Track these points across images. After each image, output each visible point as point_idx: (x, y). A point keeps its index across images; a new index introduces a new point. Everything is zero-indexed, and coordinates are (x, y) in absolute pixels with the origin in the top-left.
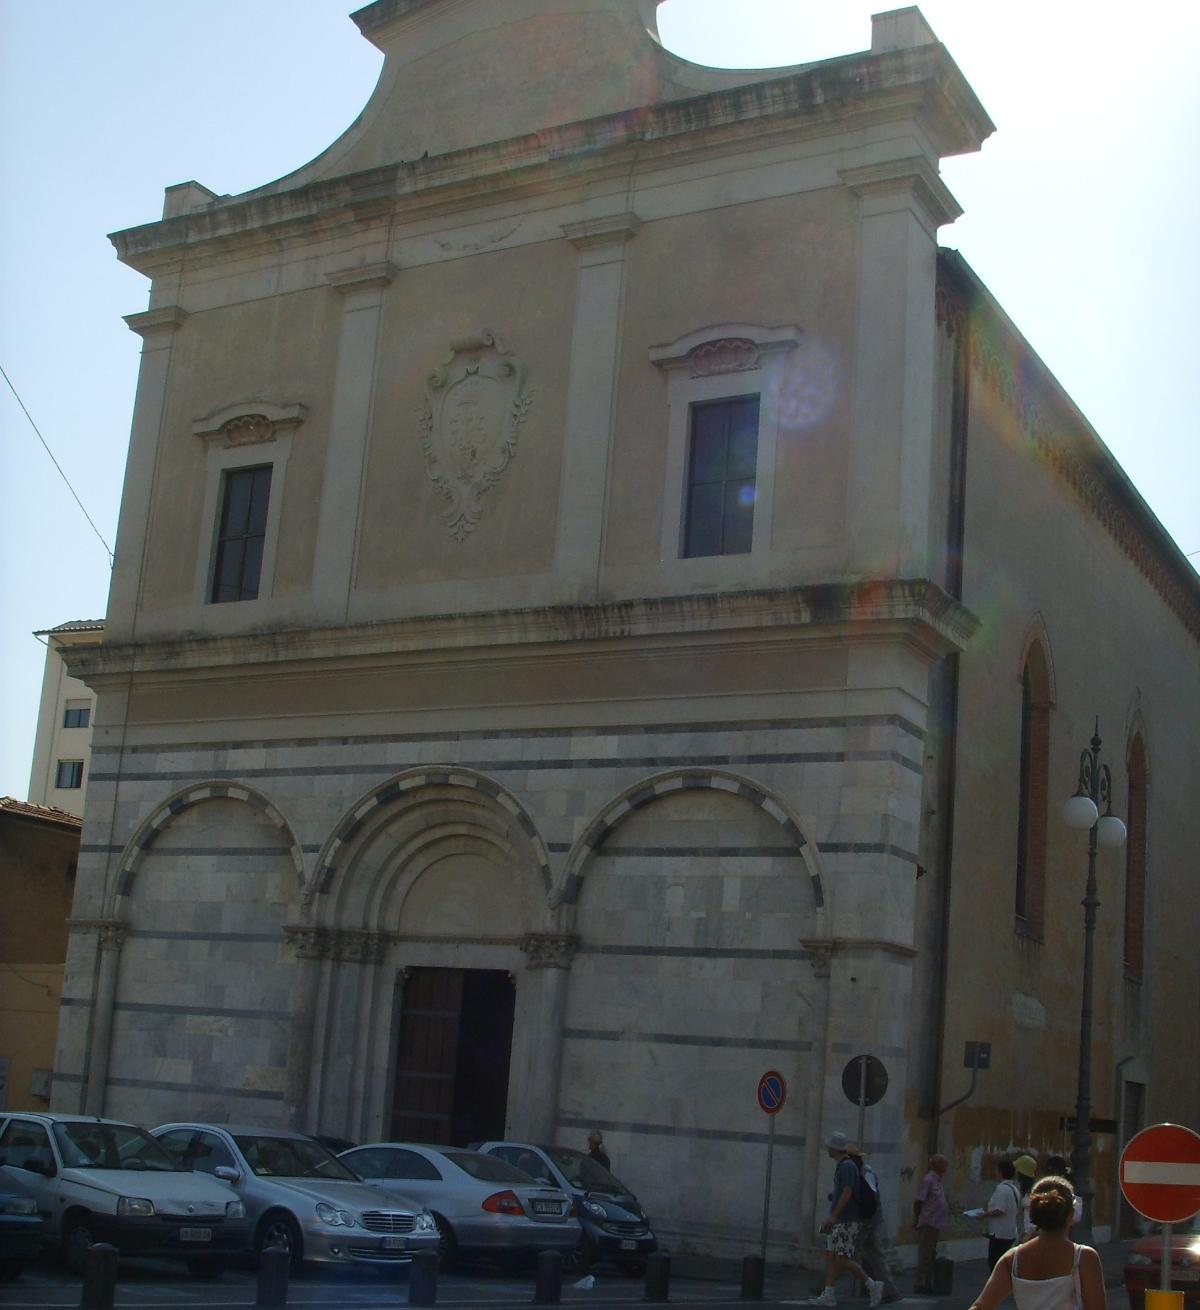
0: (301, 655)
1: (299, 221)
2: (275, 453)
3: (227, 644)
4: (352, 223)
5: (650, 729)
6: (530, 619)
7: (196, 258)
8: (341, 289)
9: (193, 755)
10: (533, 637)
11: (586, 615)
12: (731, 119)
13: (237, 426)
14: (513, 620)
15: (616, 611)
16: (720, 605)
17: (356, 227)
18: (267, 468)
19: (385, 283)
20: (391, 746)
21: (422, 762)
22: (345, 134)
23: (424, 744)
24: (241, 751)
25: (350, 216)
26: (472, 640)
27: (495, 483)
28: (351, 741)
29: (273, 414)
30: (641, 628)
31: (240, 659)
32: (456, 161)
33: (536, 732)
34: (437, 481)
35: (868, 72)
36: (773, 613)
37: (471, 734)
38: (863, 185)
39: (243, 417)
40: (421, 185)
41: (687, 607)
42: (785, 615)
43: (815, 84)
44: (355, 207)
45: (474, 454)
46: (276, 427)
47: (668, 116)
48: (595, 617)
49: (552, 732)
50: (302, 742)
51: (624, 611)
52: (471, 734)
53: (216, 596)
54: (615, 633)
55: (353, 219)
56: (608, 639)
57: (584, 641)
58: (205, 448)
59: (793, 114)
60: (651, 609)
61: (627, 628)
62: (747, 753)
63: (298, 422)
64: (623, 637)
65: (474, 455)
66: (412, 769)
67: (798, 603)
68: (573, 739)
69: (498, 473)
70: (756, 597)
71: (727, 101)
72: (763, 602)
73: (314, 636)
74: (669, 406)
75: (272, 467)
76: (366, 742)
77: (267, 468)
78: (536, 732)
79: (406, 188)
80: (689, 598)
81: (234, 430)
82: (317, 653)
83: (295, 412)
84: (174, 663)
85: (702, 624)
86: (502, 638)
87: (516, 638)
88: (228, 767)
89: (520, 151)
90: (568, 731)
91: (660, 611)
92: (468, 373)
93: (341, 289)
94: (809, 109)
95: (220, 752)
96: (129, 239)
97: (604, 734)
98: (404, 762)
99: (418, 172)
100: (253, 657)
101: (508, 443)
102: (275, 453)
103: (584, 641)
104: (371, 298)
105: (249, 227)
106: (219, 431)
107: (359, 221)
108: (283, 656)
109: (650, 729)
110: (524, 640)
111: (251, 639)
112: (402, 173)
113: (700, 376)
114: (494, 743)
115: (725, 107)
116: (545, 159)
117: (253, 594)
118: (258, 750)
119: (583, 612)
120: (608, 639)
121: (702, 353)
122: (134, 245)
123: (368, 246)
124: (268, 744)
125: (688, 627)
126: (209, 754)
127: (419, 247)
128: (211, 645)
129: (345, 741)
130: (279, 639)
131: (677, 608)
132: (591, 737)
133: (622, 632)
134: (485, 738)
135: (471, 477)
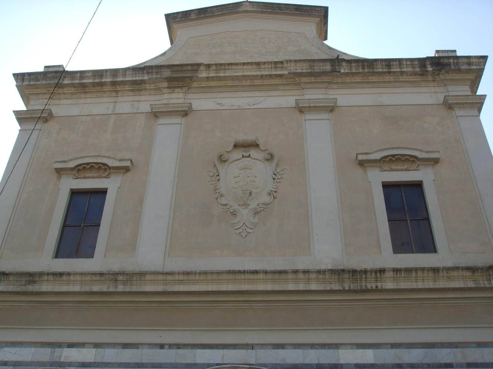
0: (135, 289)
1: (134, 83)
2: (112, 184)
3: (78, 278)
4: (164, 88)
5: (394, 346)
6: (313, 276)
7: (64, 93)
8: (156, 114)
9: (33, 350)
10: (314, 287)
11: (353, 275)
12: (387, 70)
13: (84, 168)
14: (301, 276)
15: (373, 274)
16: (441, 274)
17: (166, 91)
18: (103, 192)
19: (185, 114)
20: (199, 351)
21: (224, 362)
22: (156, 57)
23: (226, 351)
24: (74, 350)
25: (165, 84)
26: (269, 287)
27: (265, 210)
28: (166, 347)
29: (111, 163)
30: (390, 285)
31: (86, 289)
32: (234, 67)
33: (313, 346)
34: (226, 205)
35: (454, 62)
36: (474, 281)
37: (262, 346)
38: (456, 103)
39: (91, 163)
40: (212, 75)
41: (420, 274)
42: (481, 282)
43: (428, 63)
44: (170, 80)
45: (251, 194)
46: (111, 171)
47: (353, 65)
48: (358, 277)
49: (323, 346)
50: (126, 346)
51: (378, 275)
52: (262, 346)
53: (58, 254)
54: (372, 287)
55: (167, 86)
56: (366, 291)
57: (350, 291)
58: (59, 178)
59: (415, 74)
60: (397, 274)
61: (379, 285)
62: (464, 361)
63: (127, 169)
64: (377, 290)
65: (251, 195)
66: (217, 367)
67: (490, 275)
68: (340, 351)
69: (268, 204)
70: (464, 271)
71: (384, 63)
72: (468, 273)
73: (148, 277)
74: (370, 182)
75: (106, 192)
76: (179, 348)
77: (103, 192)
78: (313, 346)
79: (204, 75)
80: (423, 269)
81: (82, 169)
82: (148, 288)
83: (128, 164)
84: (30, 288)
85: (430, 284)
86: (291, 287)
87: (302, 287)
88: (62, 360)
89: (271, 68)
90: (336, 346)
91: (403, 275)
92: (243, 156)
93: (156, 114)
94: (423, 73)
95: (56, 349)
96: (26, 77)
97: (363, 348)
98: (211, 362)
99: (212, 69)
100: (96, 288)
101: (272, 191)
102: (112, 184)
103: (350, 291)
104: (177, 120)
105: (104, 80)
106: (72, 169)
107: (168, 88)
108: (120, 288)
109: (394, 346)
110: (308, 289)
111: (98, 276)
112: (202, 68)
113: (385, 171)
114: (281, 351)
115: (383, 66)
116: (286, 72)
117: (91, 256)
118: (89, 350)
119: (351, 274)
120: (366, 291)
121: (387, 160)
122: (26, 82)
123: (177, 98)
124: (97, 345)
125: (420, 285)
126: (48, 350)
127: (202, 102)
128: (65, 278)
129: (162, 346)
130: (120, 278)
131: (414, 274)
132: (354, 350)
133: (377, 287)
134: (274, 349)
135: (248, 205)
